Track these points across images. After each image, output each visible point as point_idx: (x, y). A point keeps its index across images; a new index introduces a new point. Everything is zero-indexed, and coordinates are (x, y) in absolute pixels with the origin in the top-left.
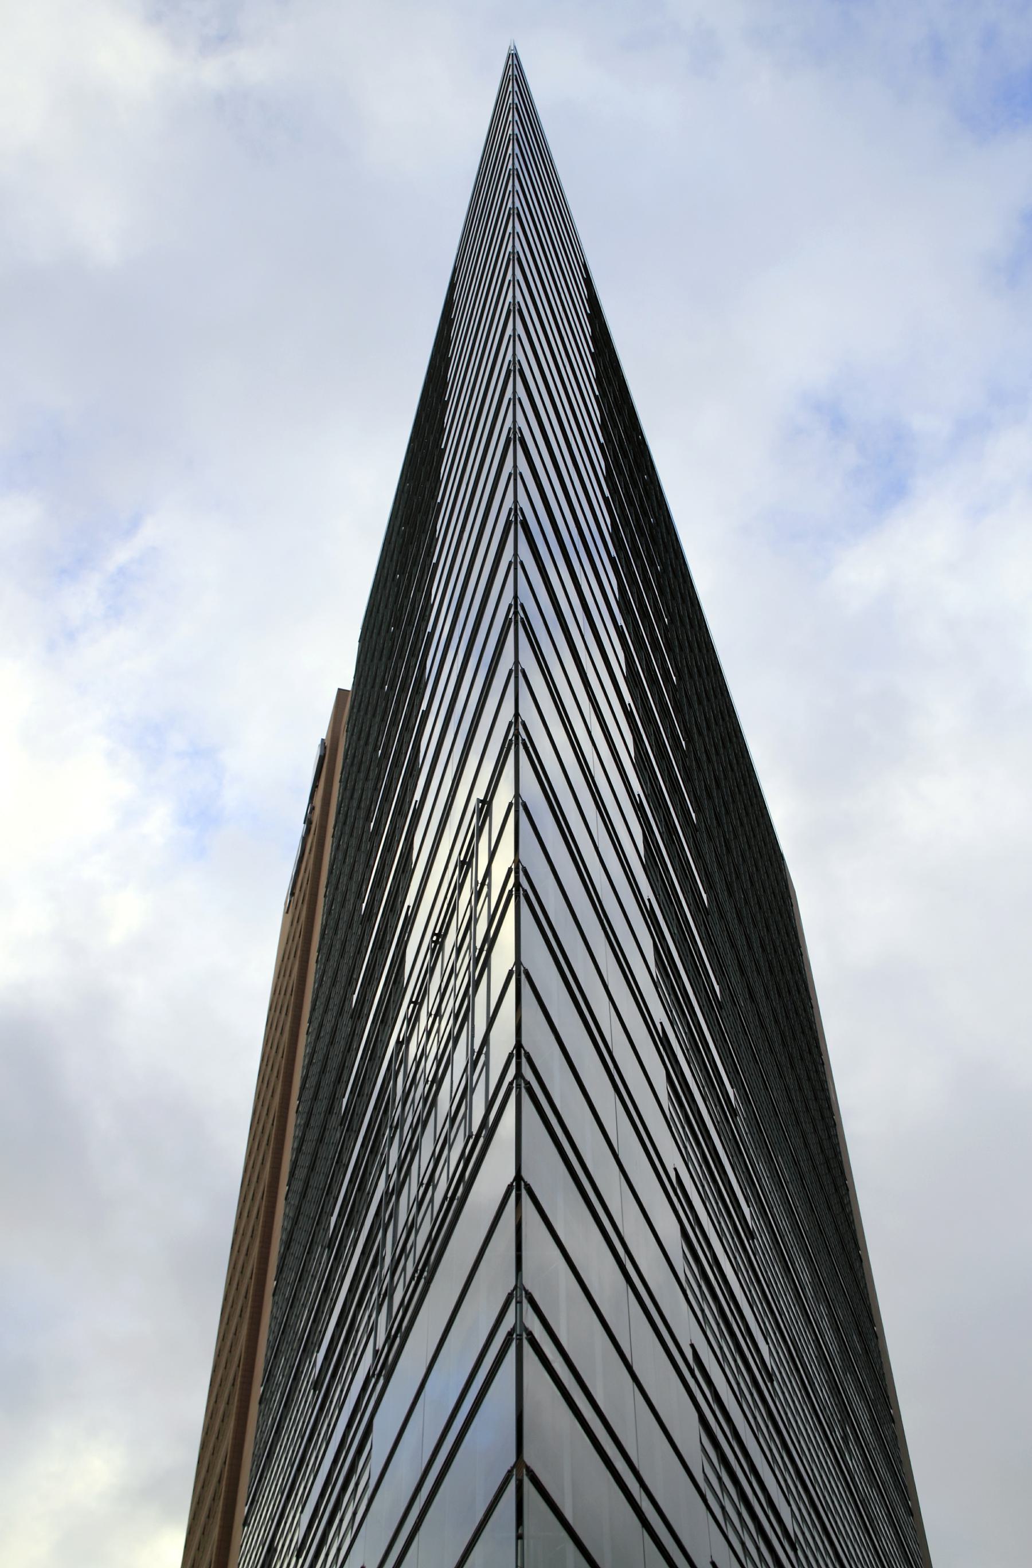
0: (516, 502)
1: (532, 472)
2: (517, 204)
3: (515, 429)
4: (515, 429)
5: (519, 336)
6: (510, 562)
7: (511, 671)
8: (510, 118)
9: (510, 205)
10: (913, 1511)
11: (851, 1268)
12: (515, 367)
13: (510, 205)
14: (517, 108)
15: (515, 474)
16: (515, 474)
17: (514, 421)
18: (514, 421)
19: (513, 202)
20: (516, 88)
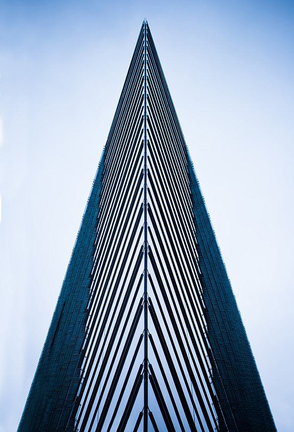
0: (146, 360)
1: (146, 44)
2: (149, 201)
3: (146, 299)
4: (146, 299)
5: (149, 228)
6: (142, 336)
7: (141, 414)
8: (143, 85)
9: (142, 167)
10: (93, 194)
11: (52, 344)
12: (146, 251)
13: (142, 167)
14: (148, 79)
15: (146, 335)
16: (146, 335)
17: (146, 293)
18: (146, 293)
19: (145, 165)
20: (148, 127)
